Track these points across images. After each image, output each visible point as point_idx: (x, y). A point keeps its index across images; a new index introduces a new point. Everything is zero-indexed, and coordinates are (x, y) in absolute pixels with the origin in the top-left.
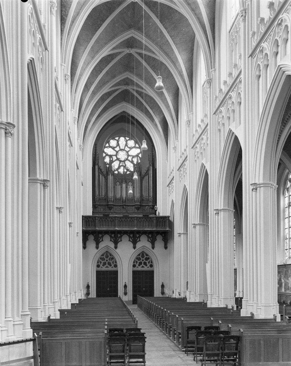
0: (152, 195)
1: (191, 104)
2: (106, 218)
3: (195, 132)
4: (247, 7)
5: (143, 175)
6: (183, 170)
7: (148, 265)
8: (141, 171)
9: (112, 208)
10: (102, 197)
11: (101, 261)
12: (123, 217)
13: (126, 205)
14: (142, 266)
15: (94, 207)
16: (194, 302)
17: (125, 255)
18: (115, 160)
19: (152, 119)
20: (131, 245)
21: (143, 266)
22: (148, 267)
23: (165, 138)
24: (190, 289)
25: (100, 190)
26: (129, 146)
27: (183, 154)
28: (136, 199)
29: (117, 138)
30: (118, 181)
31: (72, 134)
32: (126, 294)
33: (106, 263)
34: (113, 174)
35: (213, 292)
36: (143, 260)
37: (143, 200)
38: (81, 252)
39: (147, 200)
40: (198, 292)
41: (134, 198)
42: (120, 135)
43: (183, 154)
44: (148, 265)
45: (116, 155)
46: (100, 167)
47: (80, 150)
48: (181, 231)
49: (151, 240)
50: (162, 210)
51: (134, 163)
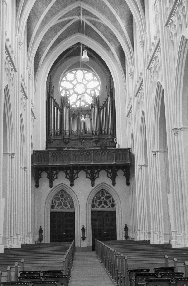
0: (112, 127)
1: (144, 24)
2: (60, 153)
3: (149, 52)
4: (143, 39)
5: (101, 106)
6: (141, 95)
7: (109, 204)
8: (99, 102)
9: (68, 142)
10: (58, 131)
11: (56, 201)
12: (79, 151)
13: (83, 139)
14: (102, 206)
15: (49, 141)
16: (159, 243)
17: (82, 192)
18: (73, 94)
19: (107, 48)
20: (89, 181)
21: (103, 206)
22: (109, 207)
23: (122, 66)
24: (153, 228)
25: (55, 125)
26: (87, 79)
27: (140, 78)
28: (94, 133)
29: (74, 72)
30: (74, 114)
31: (27, 89)
32: (84, 238)
33: (61, 203)
34: (69, 107)
35: (177, 228)
36: (103, 199)
37: (102, 133)
38: (29, 190)
39: (106, 133)
40: (163, 233)
41: (92, 131)
42: (77, 68)
43: (140, 78)
44: (109, 205)
45: (73, 89)
46: (55, 99)
47: (30, 79)
48: (142, 163)
49: (111, 175)
50: (122, 142)
51: (74, 76)
